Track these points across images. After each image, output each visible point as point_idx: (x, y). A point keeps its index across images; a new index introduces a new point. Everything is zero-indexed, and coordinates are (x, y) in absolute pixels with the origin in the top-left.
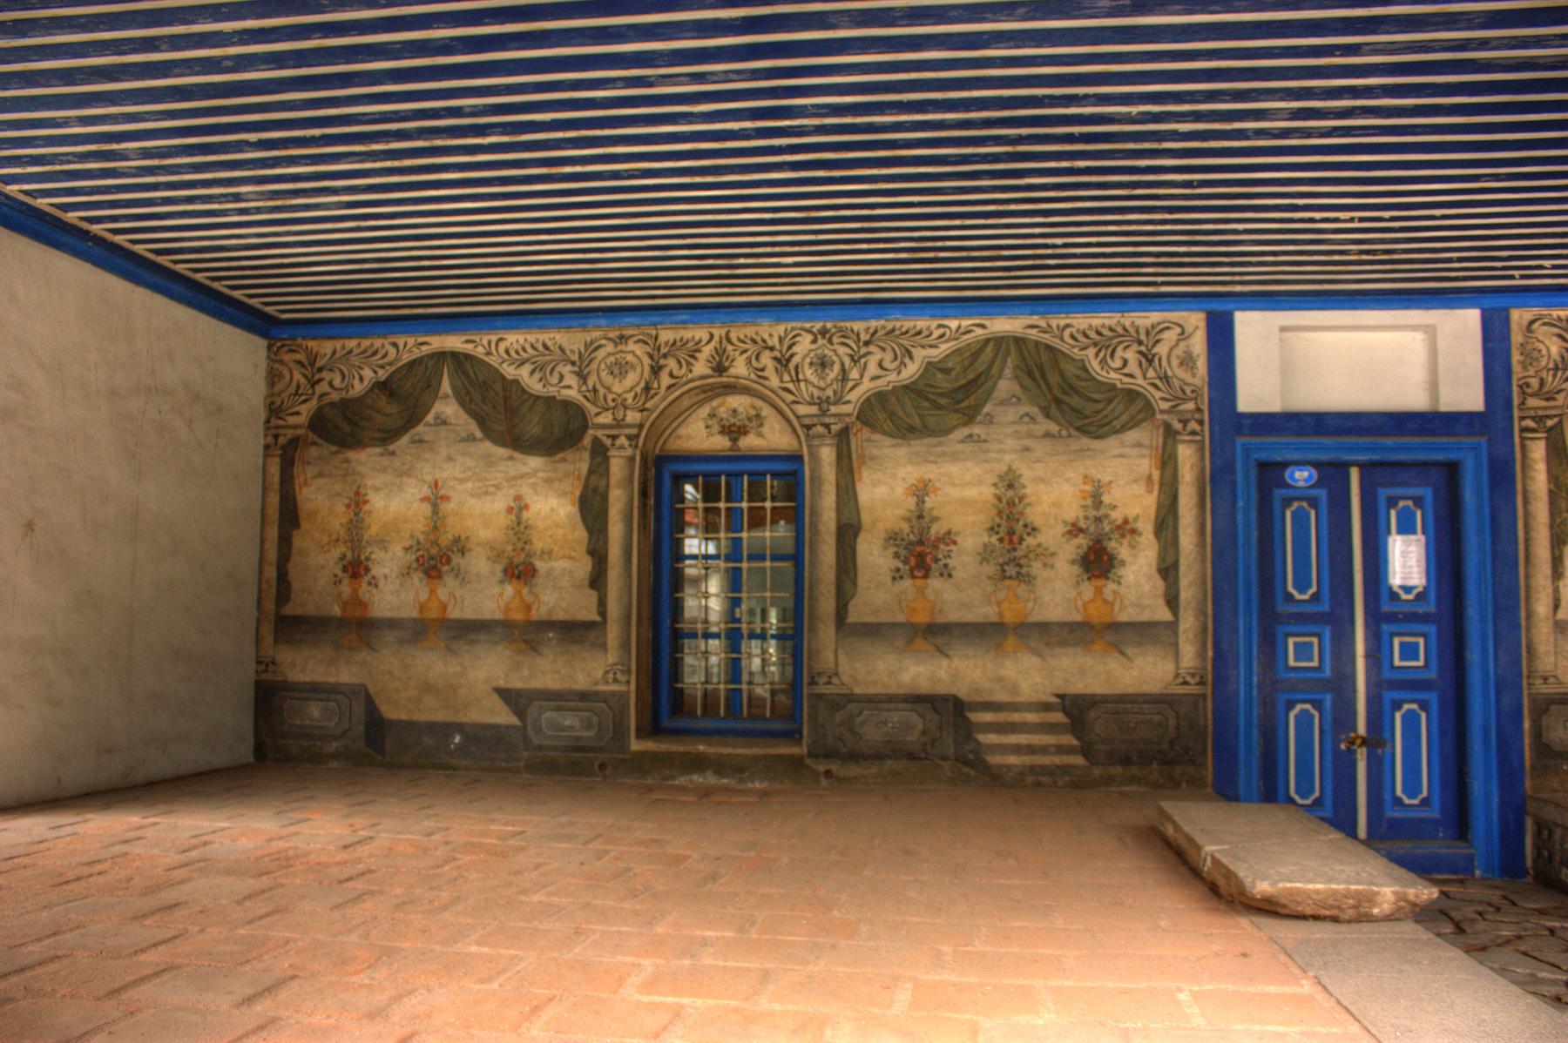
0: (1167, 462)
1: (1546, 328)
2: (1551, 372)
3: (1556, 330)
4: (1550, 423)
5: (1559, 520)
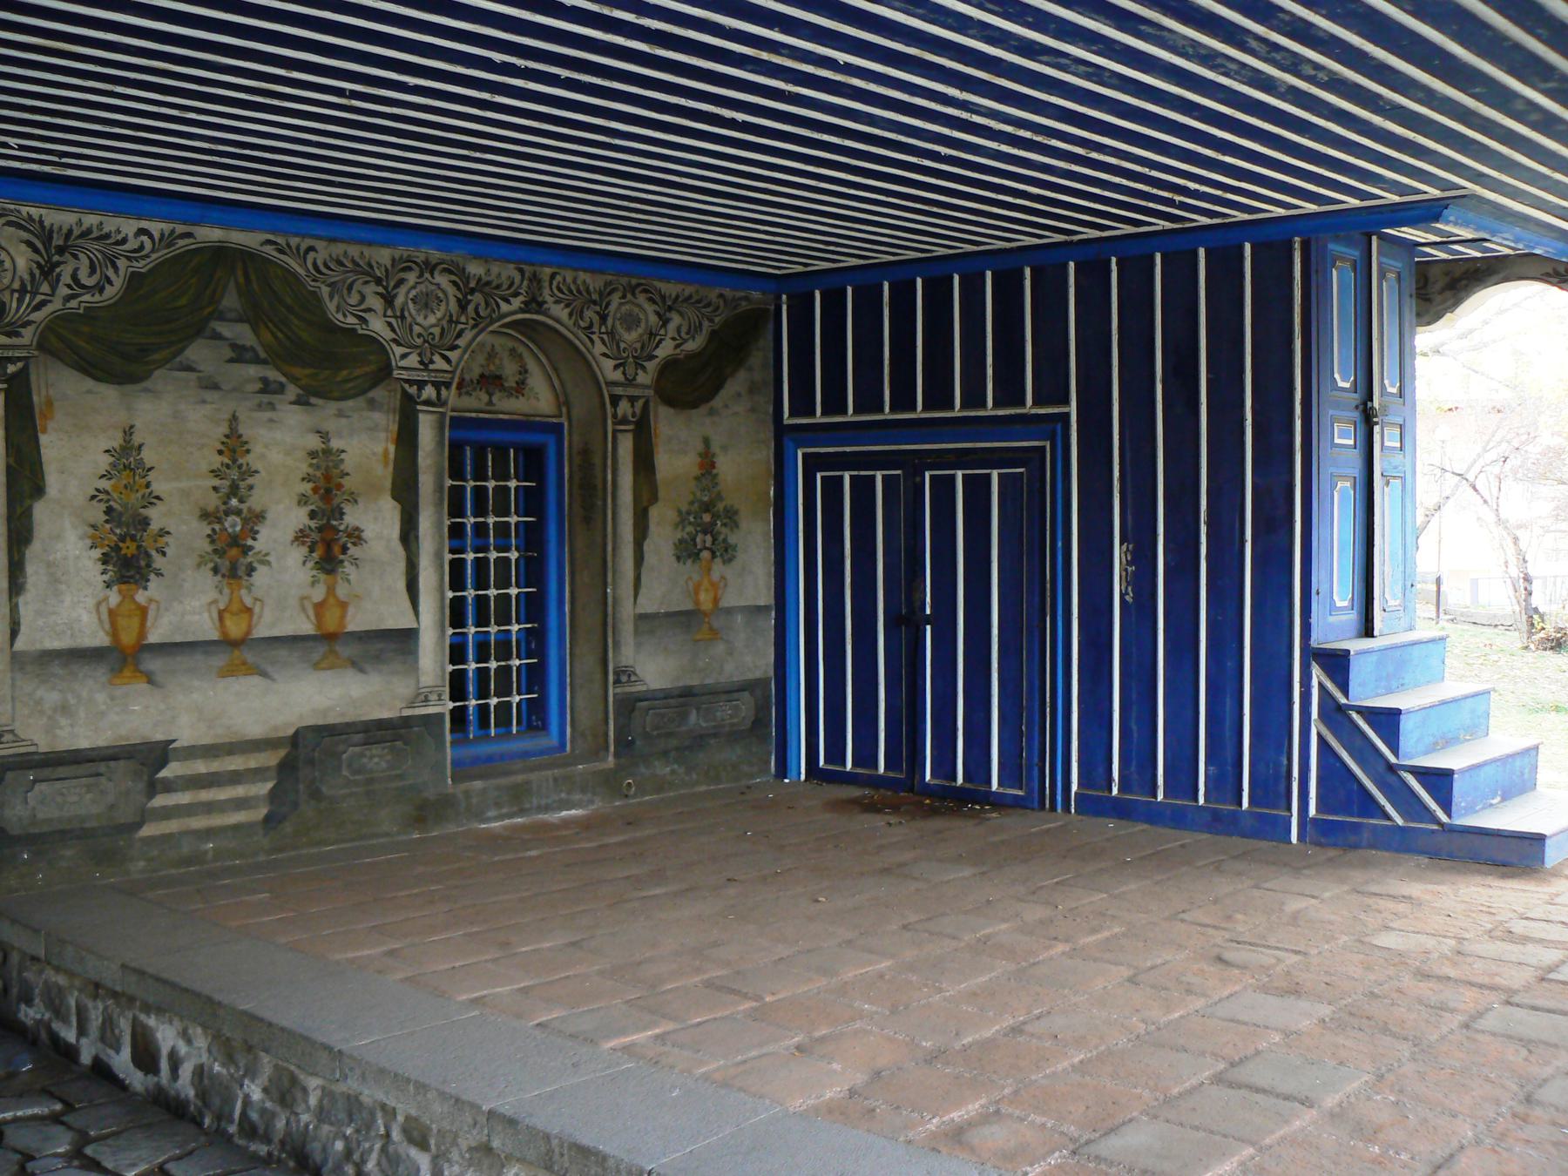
0: (407, 438)
1: (12, 229)
2: (16, 295)
3: (25, 235)
4: (11, 369)
5: (19, 510)
